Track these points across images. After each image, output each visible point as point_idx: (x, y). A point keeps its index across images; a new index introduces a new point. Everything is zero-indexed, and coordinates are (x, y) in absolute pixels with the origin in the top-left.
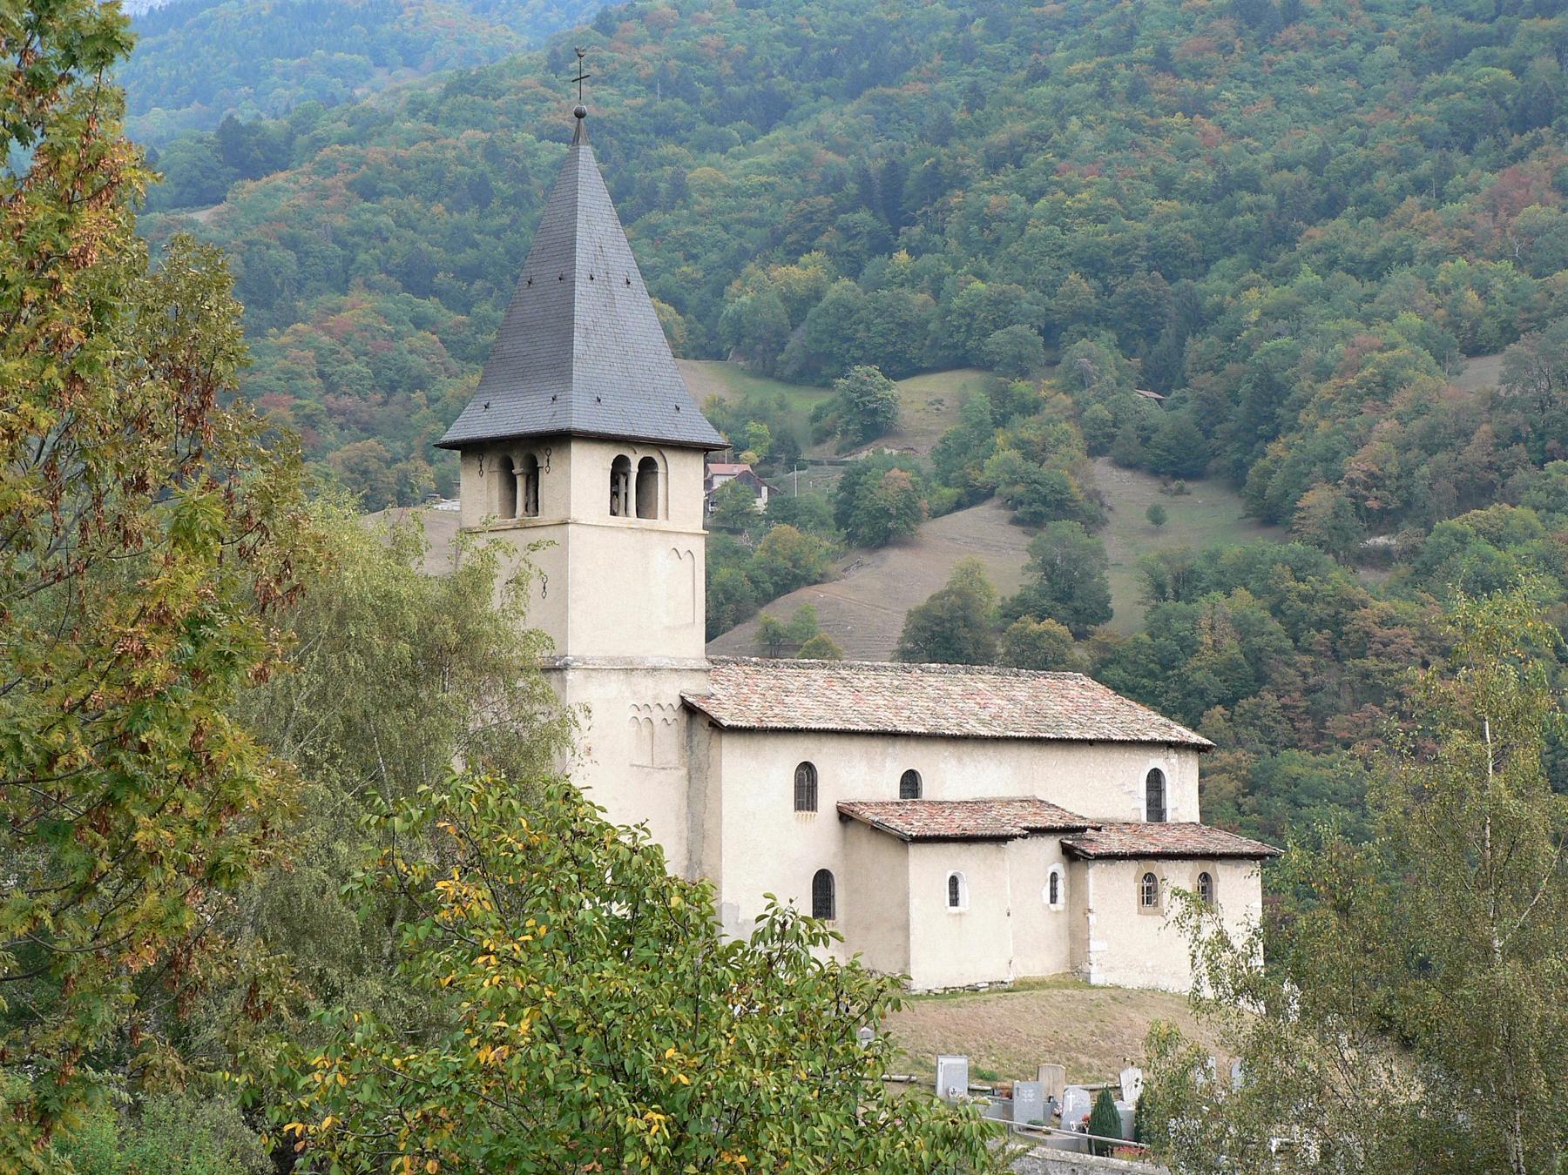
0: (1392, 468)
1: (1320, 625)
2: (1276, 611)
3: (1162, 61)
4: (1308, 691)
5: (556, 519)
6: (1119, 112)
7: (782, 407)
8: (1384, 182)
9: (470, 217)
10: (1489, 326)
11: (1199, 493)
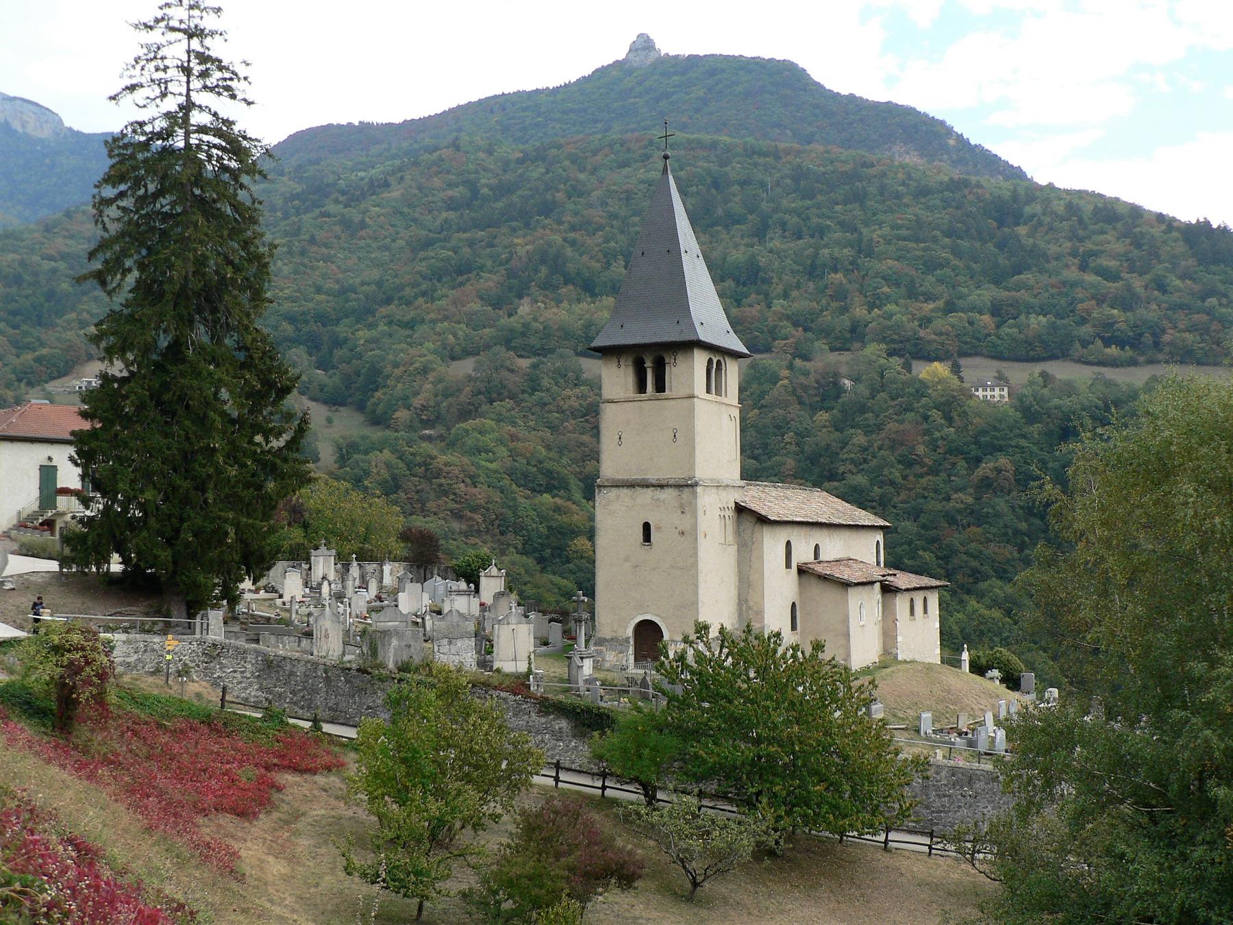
0: (432, 403)
1: (419, 465)
2: (400, 458)
3: (312, 241)
4: (417, 492)
5: (682, 393)
6: (297, 259)
7: (971, 323)
8: (408, 291)
9: (14, 289)
10: (457, 349)
11: (344, 411)
